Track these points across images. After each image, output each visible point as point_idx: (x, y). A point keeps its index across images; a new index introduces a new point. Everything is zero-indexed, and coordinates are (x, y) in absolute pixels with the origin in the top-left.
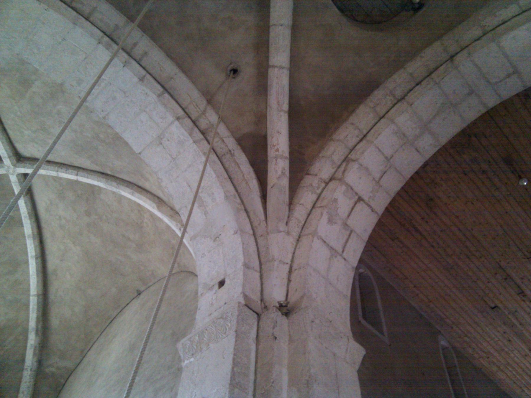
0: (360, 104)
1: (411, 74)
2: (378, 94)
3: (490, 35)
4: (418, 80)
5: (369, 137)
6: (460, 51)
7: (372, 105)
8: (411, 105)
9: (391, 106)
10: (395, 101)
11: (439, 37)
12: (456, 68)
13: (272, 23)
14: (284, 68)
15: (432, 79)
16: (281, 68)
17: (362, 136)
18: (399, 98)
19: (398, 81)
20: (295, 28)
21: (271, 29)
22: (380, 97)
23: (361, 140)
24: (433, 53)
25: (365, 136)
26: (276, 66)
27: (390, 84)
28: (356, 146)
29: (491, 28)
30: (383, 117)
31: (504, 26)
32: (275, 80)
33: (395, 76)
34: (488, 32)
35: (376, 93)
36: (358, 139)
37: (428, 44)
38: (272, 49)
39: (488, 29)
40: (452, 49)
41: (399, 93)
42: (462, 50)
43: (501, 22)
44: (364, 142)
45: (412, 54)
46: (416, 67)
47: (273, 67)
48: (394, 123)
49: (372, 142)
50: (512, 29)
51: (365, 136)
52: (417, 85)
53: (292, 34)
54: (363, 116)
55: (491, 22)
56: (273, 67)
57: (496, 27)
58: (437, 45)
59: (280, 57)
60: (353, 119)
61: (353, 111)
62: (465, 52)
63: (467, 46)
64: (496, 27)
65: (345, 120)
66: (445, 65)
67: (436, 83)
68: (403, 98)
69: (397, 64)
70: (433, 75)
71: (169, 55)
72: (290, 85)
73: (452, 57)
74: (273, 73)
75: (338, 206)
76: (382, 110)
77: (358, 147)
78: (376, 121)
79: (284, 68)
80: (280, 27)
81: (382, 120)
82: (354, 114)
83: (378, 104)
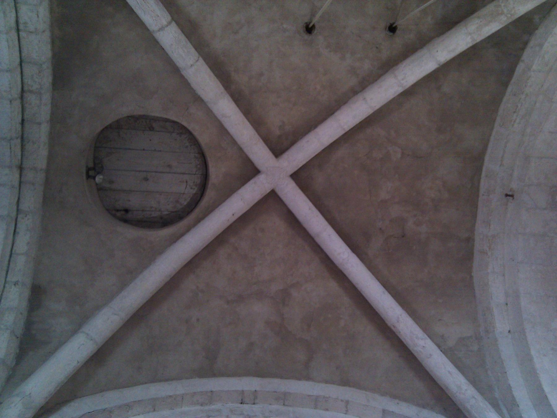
0: (54, 56)
1: (40, 124)
2: (47, 79)
3: (14, 214)
4: (27, 125)
5: (14, 34)
6: (20, 179)
7: (45, 66)
8: (11, 101)
9: (25, 81)
10: (26, 88)
11: (48, 171)
12: (10, 167)
13: (201, 61)
14: (159, 30)
15: (17, 138)
16: (162, 29)
17: (21, 27)
18: (25, 95)
19: (41, 108)
20: (176, 70)
21: (196, 54)
22: (42, 79)
23: (17, 22)
24: (39, 156)
25: (18, 30)
26: (167, 26)
27: (47, 97)
28: (17, 12)
29: (19, 219)
30: (21, 65)
31: (12, 232)
32: (159, 12)
33: (49, 106)
34: (17, 214)
35: (50, 79)
36: (21, 21)
37: (51, 157)
38: (183, 38)
39: (20, 216)
40: (29, 176)
41: (31, 99)
42: (20, 183)
43: (17, 230)
44: (13, 24)
45: (54, 138)
46: (41, 134)
47: (169, 23)
48: (7, 71)
49: (7, 33)
50: (6, 238)
51: (18, 30)
52: (23, 120)
53: (175, 64)
54: (40, 48)
55: (25, 223)
56: (169, 23)
57: (16, 225)
58: (42, 163)
59: (171, 38)
60: (46, 37)
61: (53, 42)
62: (17, 184)
63: (20, 189)
64: (16, 225)
65: (52, 26)
66: (20, 157)
67: (11, 139)
68: (22, 97)
69: (58, 119)
70: (19, 140)
71: (490, 135)
72: (137, 17)
73: (21, 168)
74: (164, 17)
75: (510, 336)
76: (29, 70)
77: (13, 15)
78: (23, 55)
79: (159, 30)
80: (191, 63)
81: (18, 60)
82: (49, 40)
83: (40, 72)
